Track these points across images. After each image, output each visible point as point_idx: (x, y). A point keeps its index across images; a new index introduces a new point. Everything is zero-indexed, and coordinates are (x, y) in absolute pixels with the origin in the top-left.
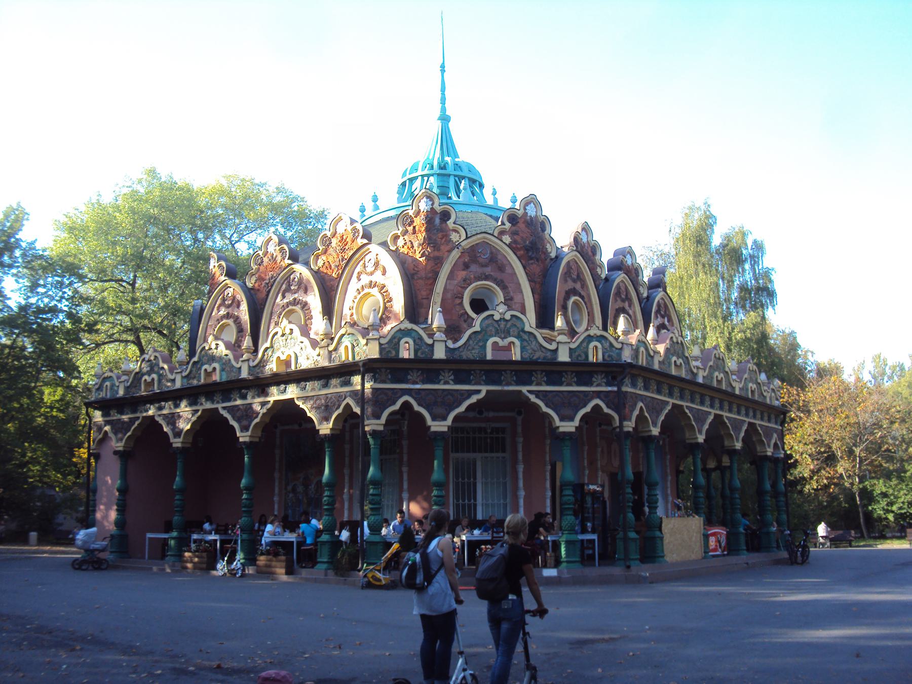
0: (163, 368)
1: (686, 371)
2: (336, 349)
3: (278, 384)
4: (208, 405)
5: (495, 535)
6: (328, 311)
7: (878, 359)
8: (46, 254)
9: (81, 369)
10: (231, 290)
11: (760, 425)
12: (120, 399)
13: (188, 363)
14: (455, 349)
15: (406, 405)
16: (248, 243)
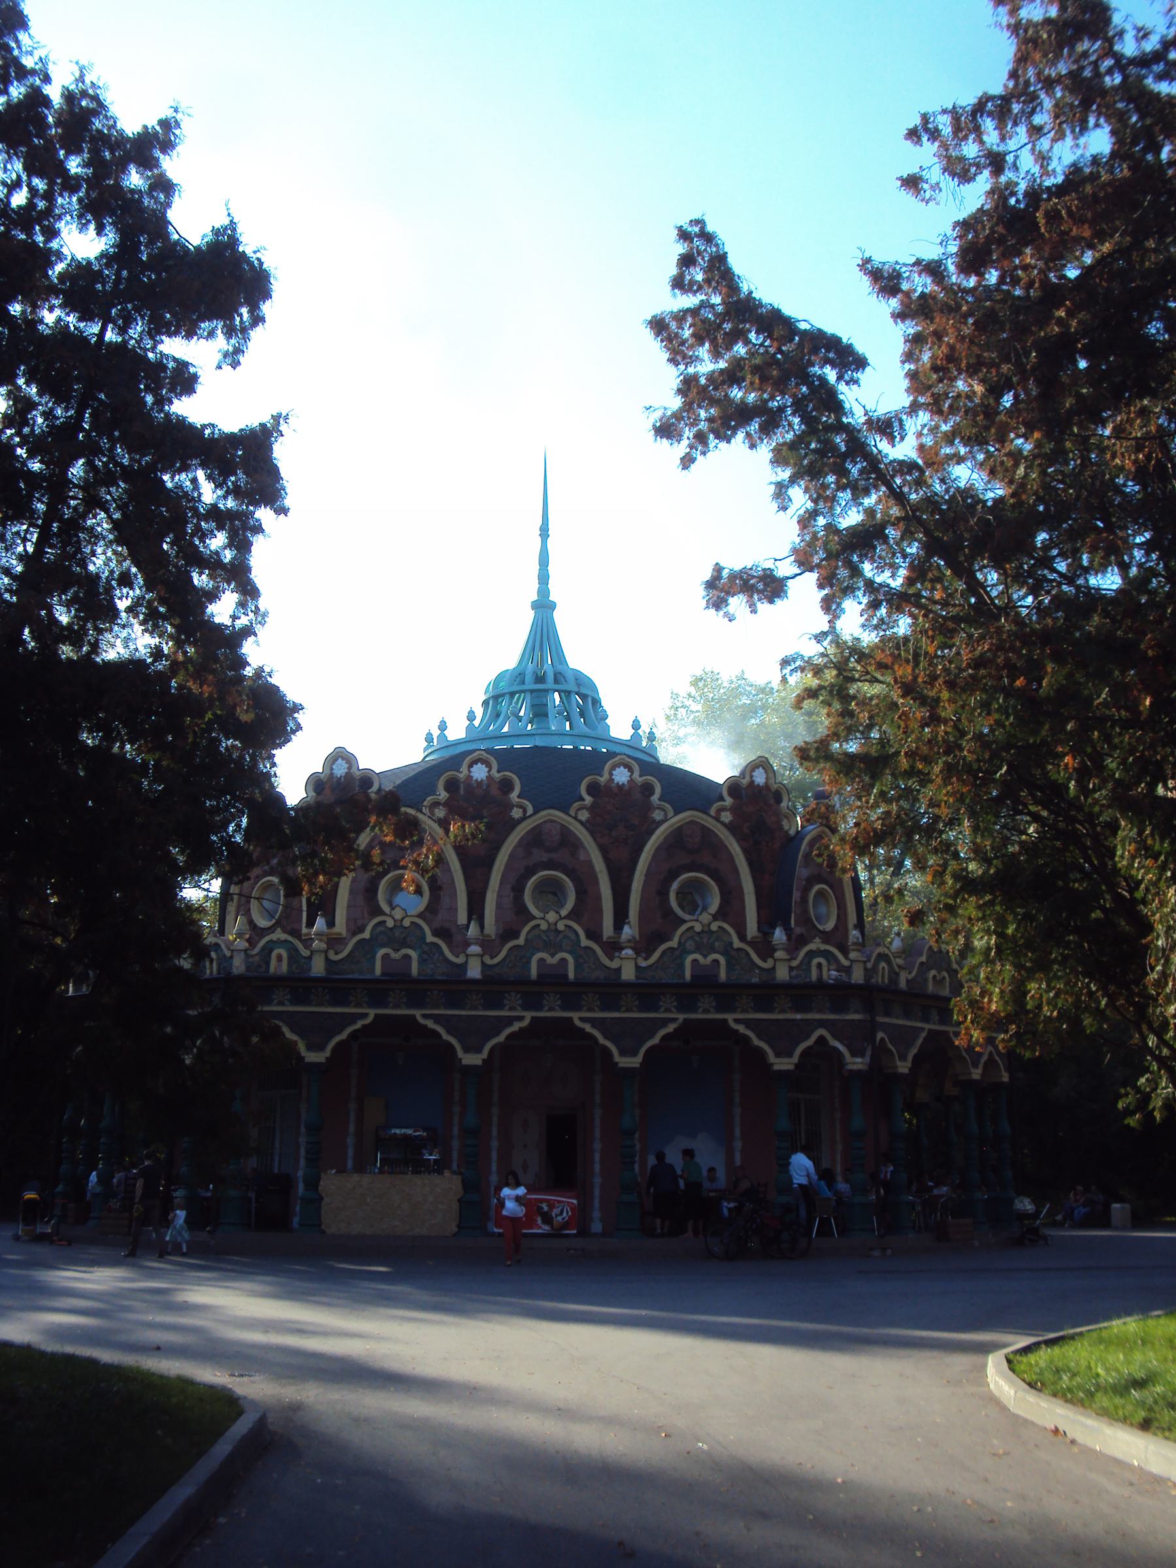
15: (821, 1039)
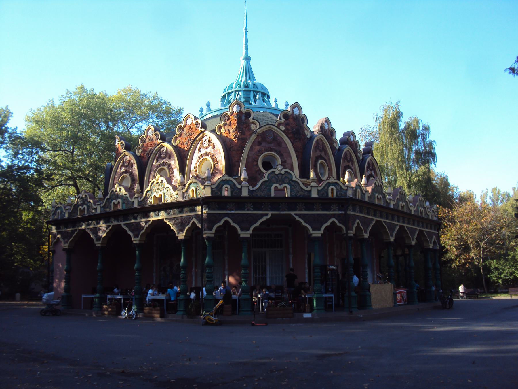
0: (90, 202)
1: (384, 201)
2: (187, 191)
3: (154, 211)
4: (116, 223)
5: (276, 294)
6: (182, 170)
7: (494, 190)
8: (22, 136)
9: (43, 201)
10: (128, 157)
11: (426, 231)
12: (66, 219)
13: (104, 199)
14: (253, 191)
15: (226, 222)
16: (137, 128)
